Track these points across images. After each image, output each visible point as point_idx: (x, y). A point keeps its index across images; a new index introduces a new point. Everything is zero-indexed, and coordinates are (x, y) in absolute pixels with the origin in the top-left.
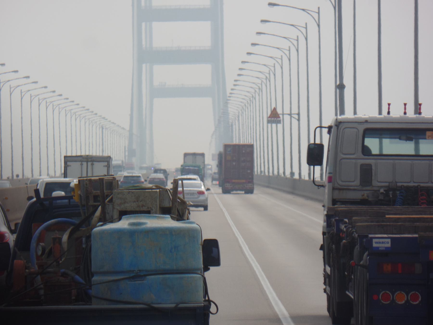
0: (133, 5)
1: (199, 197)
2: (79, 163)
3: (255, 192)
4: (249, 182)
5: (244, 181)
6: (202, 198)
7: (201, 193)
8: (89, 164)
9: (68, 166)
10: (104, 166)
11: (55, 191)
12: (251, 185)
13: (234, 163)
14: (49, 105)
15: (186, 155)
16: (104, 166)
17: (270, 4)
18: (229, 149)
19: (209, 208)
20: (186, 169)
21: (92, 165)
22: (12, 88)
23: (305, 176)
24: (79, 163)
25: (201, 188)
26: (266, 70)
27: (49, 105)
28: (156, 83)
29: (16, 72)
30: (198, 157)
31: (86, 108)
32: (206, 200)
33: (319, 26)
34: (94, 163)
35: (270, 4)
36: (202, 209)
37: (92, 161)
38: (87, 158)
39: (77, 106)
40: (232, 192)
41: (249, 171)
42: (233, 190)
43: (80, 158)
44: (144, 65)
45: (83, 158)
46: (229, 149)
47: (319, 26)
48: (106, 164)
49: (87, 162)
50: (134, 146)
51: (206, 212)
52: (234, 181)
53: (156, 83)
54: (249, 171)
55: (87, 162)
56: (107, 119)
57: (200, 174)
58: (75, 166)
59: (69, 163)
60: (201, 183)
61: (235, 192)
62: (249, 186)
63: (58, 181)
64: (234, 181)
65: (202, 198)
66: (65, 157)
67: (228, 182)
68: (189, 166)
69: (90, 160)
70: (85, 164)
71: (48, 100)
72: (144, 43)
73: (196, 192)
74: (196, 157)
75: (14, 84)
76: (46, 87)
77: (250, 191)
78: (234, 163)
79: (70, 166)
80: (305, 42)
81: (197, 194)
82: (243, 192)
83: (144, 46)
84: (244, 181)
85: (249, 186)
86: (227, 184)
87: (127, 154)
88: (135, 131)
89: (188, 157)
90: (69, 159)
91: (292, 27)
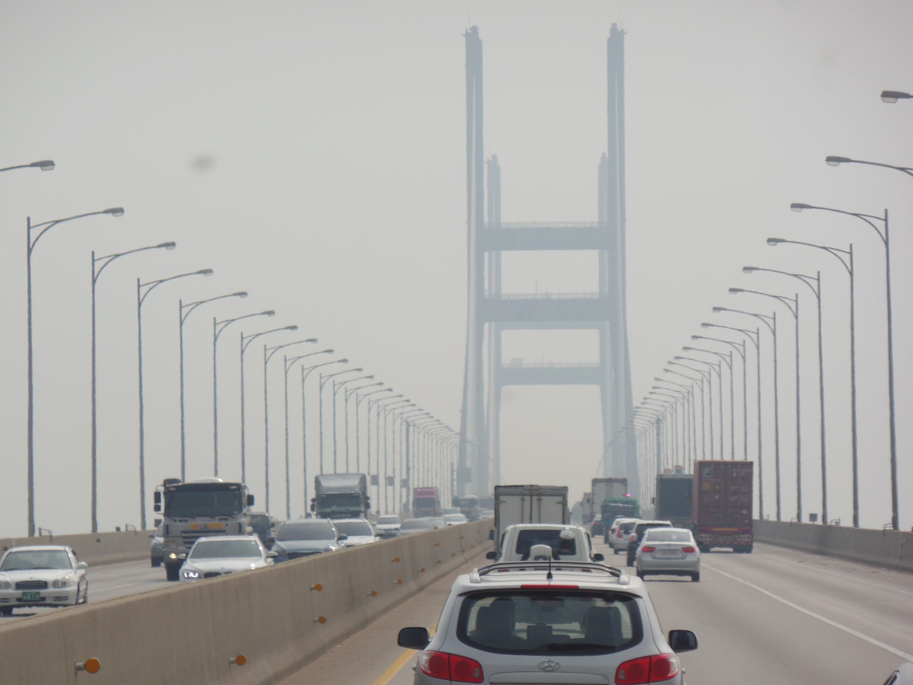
0: (469, 223)
1: (684, 558)
2: (521, 497)
3: (754, 550)
4: (745, 532)
5: (735, 529)
6: (690, 558)
7: (689, 550)
8: (535, 498)
9: (501, 502)
10: (557, 503)
11: (533, 544)
12: (748, 538)
13: (717, 497)
15: (595, 482)
16: (557, 503)
17: (732, 290)
18: (707, 471)
19: (701, 578)
20: (611, 506)
21: (539, 500)
22: (349, 391)
24: (518, 498)
25: (689, 541)
28: (506, 360)
29: (313, 340)
30: (616, 486)
31: (412, 402)
32: (697, 562)
33: (819, 297)
34: (542, 497)
35: (732, 290)
36: (689, 578)
37: (538, 495)
38: (532, 490)
39: (388, 394)
40: (712, 549)
41: (745, 512)
42: (714, 546)
43: (520, 489)
44: (486, 325)
45: (525, 490)
46: (707, 471)
47: (851, 273)
48: (560, 499)
49: (531, 495)
50: (469, 464)
51: (695, 584)
52: (715, 529)
53: (506, 360)
54: (745, 512)
55: (531, 495)
56: (432, 417)
57: (641, 513)
58: (511, 504)
59: (502, 498)
60: (328, 521)
61: (717, 549)
62: (744, 538)
63: (544, 529)
64: (715, 529)
65: (690, 558)
66: (497, 488)
67: (705, 531)
68: (616, 502)
69: (535, 492)
70: (527, 498)
71: (360, 392)
72: (486, 286)
73: (680, 548)
74: (612, 485)
75: (308, 362)
76: (360, 370)
77: (746, 548)
78: (717, 497)
79: (505, 502)
80: (884, 249)
81: (683, 552)
82: (731, 550)
83: (487, 293)
84: (735, 529)
85: (744, 538)
86: (704, 535)
87: (455, 477)
88: (470, 435)
89: (599, 485)
90: (501, 490)
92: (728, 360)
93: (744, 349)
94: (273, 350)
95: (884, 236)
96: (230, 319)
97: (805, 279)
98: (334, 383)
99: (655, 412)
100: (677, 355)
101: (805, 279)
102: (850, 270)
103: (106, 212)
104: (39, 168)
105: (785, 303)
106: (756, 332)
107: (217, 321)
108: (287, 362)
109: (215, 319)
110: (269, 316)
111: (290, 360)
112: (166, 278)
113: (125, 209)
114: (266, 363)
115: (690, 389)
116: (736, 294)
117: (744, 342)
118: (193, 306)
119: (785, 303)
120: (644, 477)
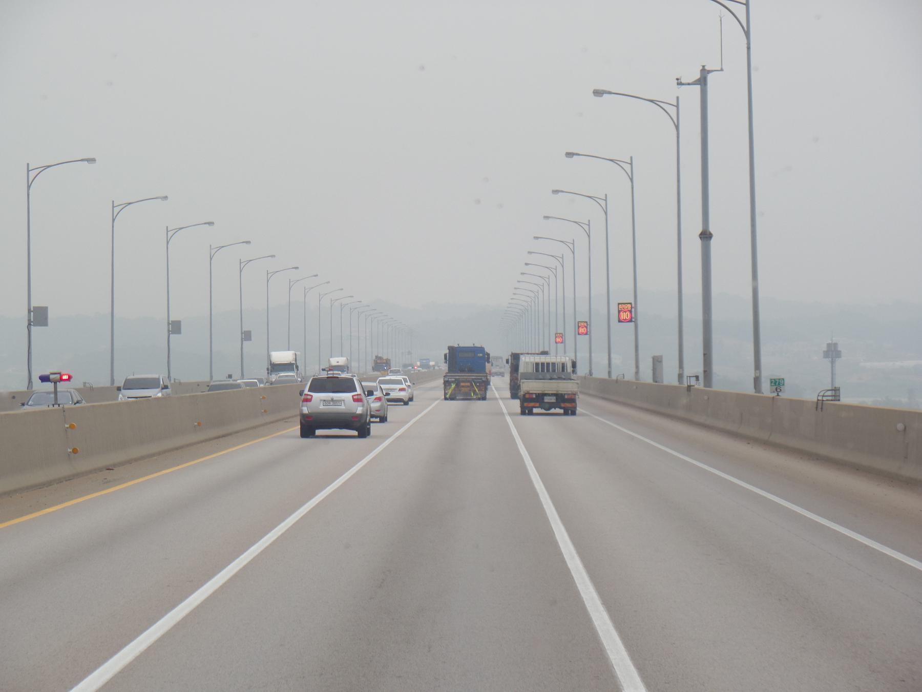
14: (293, 284)
22: (292, 281)
23: (624, 375)
26: (532, 295)
27: (293, 284)
33: (677, 127)
47: (677, 127)
91: (611, 162)
92: (542, 288)
93: (574, 247)
94: (121, 207)
95: (630, 174)
96: (221, 246)
97: (618, 162)
98: (113, 204)
99: (516, 314)
100: (546, 215)
101: (618, 162)
102: (676, 124)
103: (205, 223)
104: (208, 225)
105: (661, 107)
106: (588, 223)
107: (242, 261)
108: (269, 275)
109: (167, 227)
110: (162, 200)
111: (292, 281)
112: (133, 201)
113: (97, 159)
114: (241, 271)
115: (526, 307)
116: (557, 194)
117: (538, 290)
118: (125, 205)
119: (661, 107)
120: (450, 380)
